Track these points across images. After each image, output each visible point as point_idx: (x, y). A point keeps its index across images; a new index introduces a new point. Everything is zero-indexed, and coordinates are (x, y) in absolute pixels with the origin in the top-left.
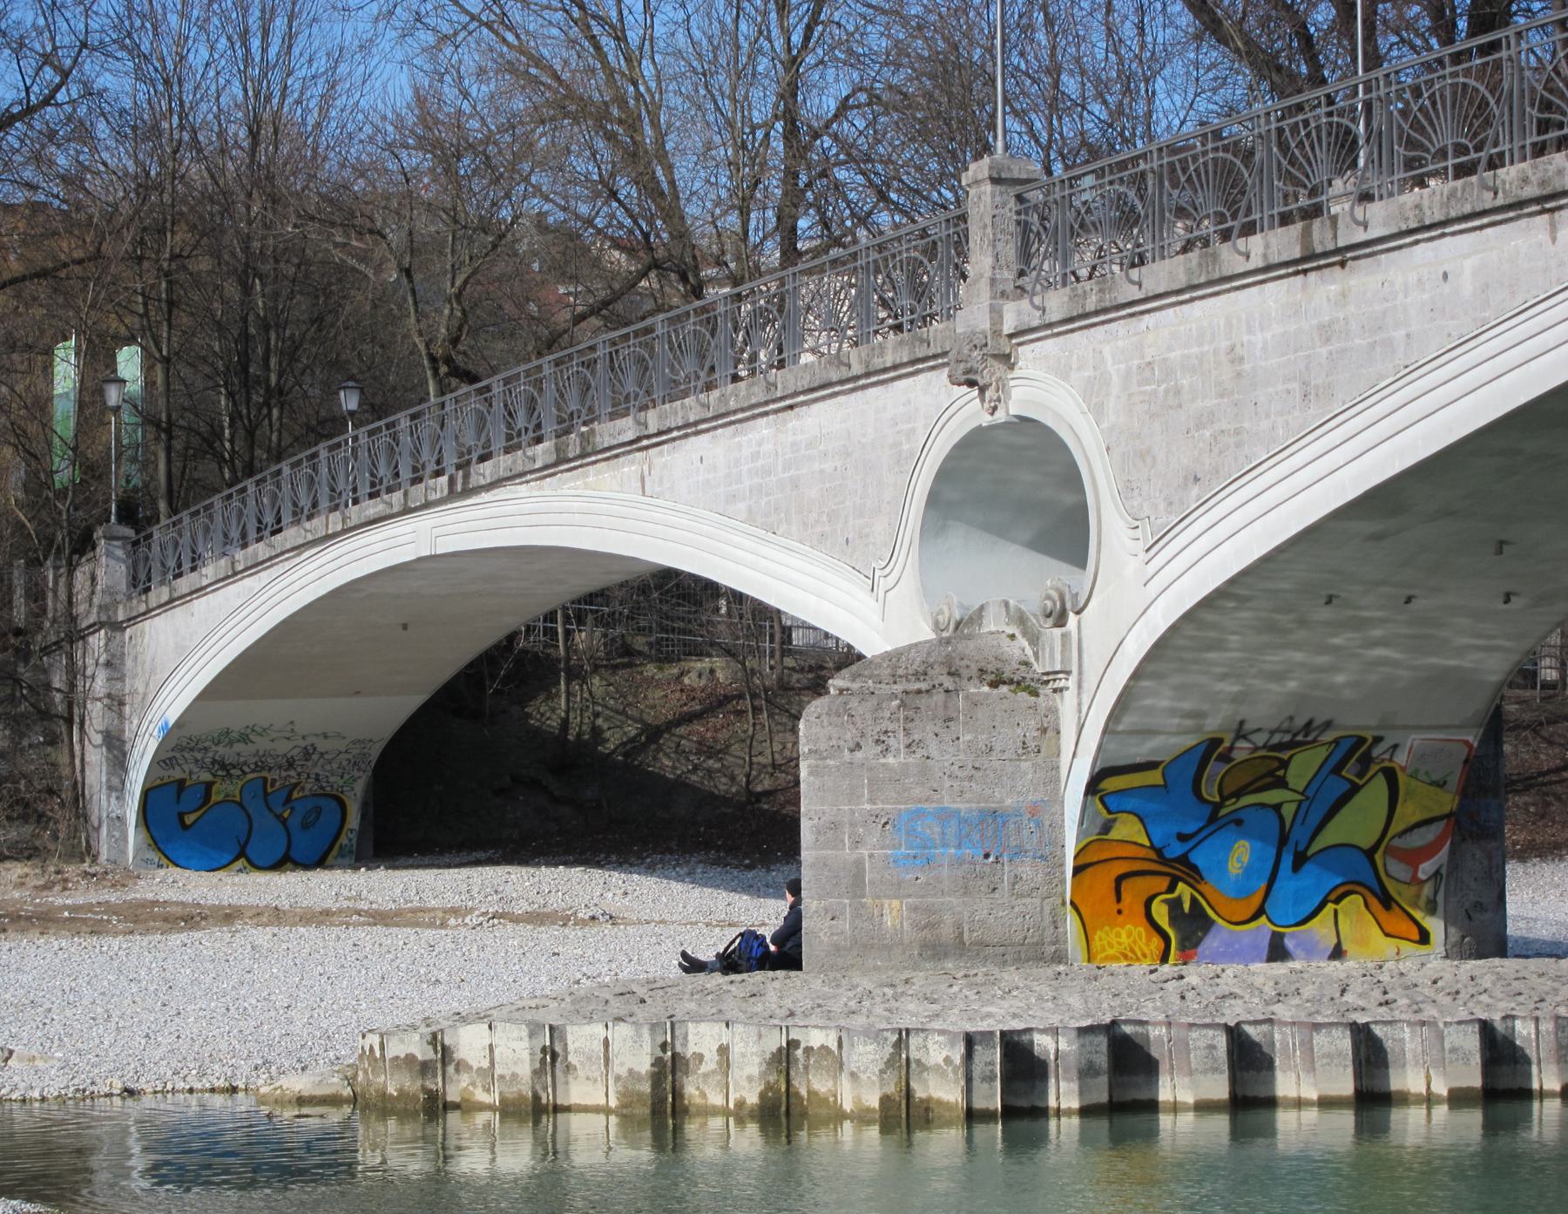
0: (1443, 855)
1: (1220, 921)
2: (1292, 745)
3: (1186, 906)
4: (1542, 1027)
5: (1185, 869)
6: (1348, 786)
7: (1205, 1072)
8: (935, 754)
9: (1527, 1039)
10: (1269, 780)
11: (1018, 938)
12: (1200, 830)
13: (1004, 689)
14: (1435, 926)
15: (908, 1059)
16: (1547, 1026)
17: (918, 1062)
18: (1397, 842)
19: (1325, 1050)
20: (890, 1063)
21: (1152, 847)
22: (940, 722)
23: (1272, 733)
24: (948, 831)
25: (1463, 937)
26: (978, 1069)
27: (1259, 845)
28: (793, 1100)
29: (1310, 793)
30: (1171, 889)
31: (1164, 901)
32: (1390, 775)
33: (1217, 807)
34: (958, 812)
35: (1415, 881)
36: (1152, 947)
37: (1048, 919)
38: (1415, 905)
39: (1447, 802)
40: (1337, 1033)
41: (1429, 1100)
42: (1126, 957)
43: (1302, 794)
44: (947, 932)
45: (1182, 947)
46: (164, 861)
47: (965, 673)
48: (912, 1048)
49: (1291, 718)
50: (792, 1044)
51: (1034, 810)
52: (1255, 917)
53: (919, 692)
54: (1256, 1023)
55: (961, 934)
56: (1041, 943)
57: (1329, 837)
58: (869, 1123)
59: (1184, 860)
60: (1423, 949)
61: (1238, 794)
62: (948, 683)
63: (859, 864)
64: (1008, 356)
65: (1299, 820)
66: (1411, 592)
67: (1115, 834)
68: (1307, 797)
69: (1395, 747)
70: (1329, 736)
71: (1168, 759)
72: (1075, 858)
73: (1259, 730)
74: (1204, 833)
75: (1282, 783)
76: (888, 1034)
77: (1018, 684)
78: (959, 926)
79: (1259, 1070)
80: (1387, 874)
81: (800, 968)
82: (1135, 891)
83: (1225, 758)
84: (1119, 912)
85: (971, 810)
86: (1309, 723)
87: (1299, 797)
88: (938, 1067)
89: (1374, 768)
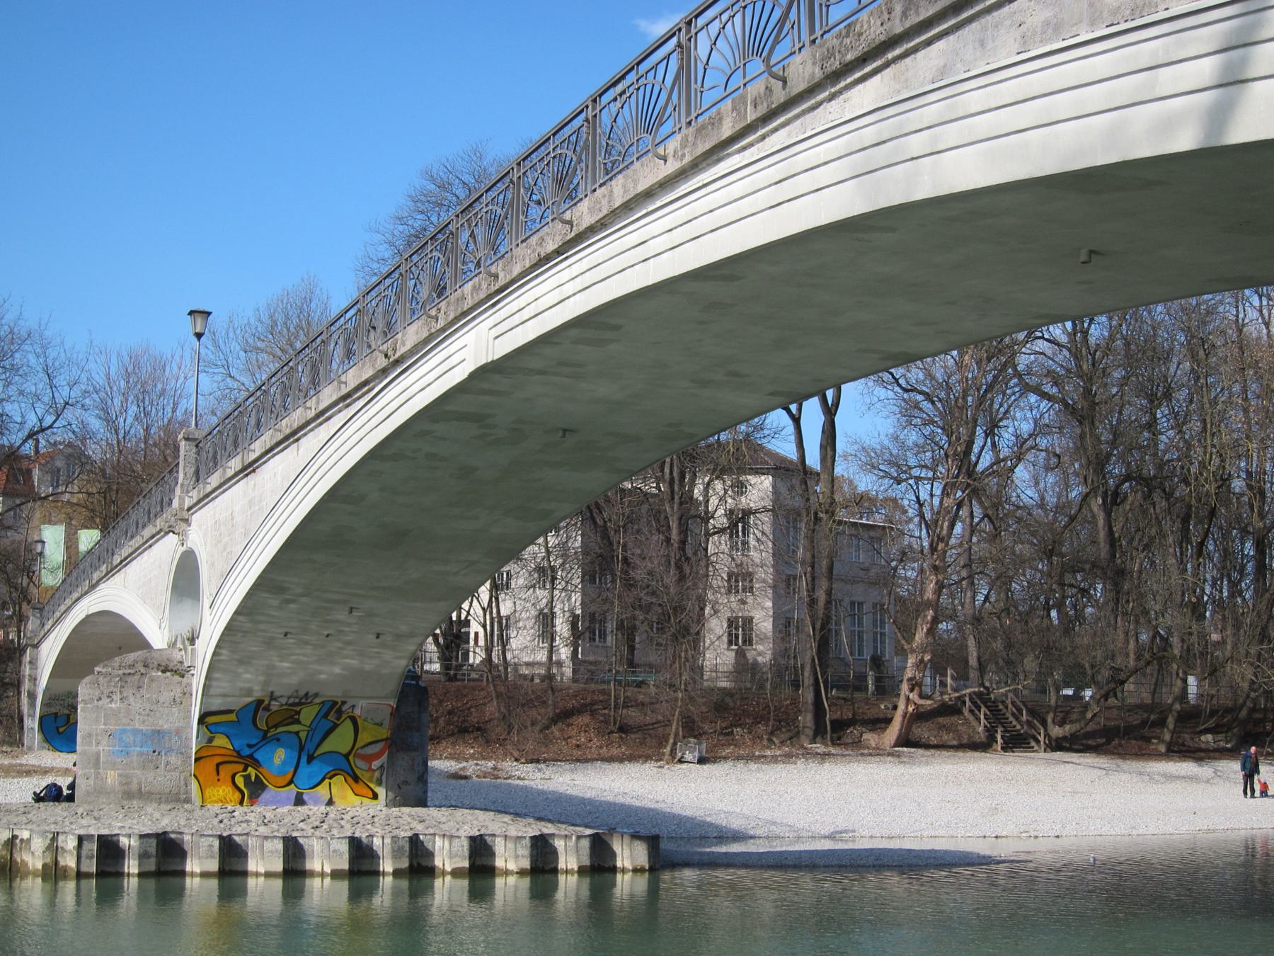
0: (384, 758)
1: (270, 786)
2: (300, 704)
3: (253, 778)
4: (386, 841)
5: (252, 761)
6: (332, 724)
7: (207, 858)
8: (133, 703)
9: (378, 847)
10: (290, 720)
11: (167, 791)
12: (257, 744)
13: (168, 674)
14: (381, 791)
15: (57, 846)
16: (388, 841)
17: (62, 848)
18: (359, 751)
19: (270, 849)
20: (48, 848)
21: (234, 750)
22: (135, 688)
23: (289, 698)
24: (137, 739)
25: (396, 797)
26: (84, 852)
27: (289, 751)
28: (13, 864)
29: (313, 727)
30: (245, 770)
31: (242, 776)
32: (354, 720)
33: (266, 732)
34: (142, 730)
35: (370, 769)
36: (236, 797)
37: (182, 783)
38: (371, 781)
39: (384, 733)
40: (276, 841)
41: (323, 875)
42: (221, 801)
43: (309, 727)
44: (134, 787)
45: (251, 798)
46: (51, 748)
47: (151, 666)
48: (60, 841)
49: (297, 691)
50: (15, 837)
51: (178, 731)
52: (289, 784)
53: (130, 674)
54: (239, 835)
55: (141, 788)
56: (179, 793)
57: (325, 747)
58: (38, 876)
59: (251, 756)
60: (374, 802)
61: (276, 726)
62: (143, 670)
63: (98, 754)
64: (188, 520)
65: (309, 738)
66: (288, 630)
67: (215, 743)
68: (312, 730)
69: (354, 706)
70: (318, 700)
71: (238, 708)
72: (196, 753)
73: (281, 696)
74: (261, 744)
75: (298, 722)
76: (48, 834)
77: (175, 672)
78: (140, 784)
79: (239, 857)
80: (356, 766)
81: (74, 801)
82: (226, 771)
83: (267, 709)
84: (219, 780)
85: (147, 730)
86: (307, 694)
87: (307, 729)
88: (70, 850)
89: (344, 716)
